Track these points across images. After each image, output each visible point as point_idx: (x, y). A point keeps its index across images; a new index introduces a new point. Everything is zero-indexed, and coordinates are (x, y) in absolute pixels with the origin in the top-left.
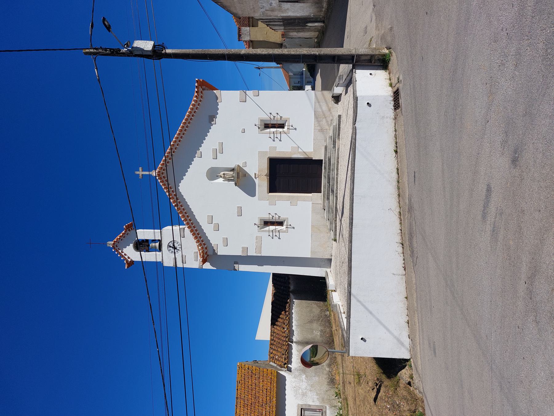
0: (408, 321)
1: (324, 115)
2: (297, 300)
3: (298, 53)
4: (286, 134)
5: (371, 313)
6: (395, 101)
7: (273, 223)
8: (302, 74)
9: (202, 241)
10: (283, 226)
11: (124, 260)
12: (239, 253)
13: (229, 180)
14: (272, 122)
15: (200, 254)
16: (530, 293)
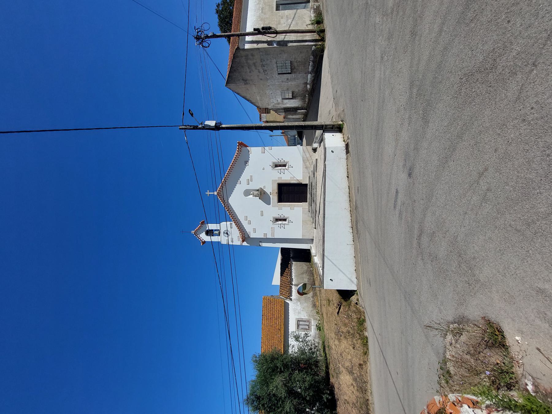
0: (356, 269)
1: (308, 159)
2: (294, 262)
3: (293, 125)
5: (335, 266)
6: (346, 149)
7: (280, 220)
8: (294, 136)
9: (242, 230)
10: (286, 221)
11: (200, 241)
12: (262, 236)
13: (256, 196)
14: (279, 164)
15: (241, 237)
16: (419, 244)
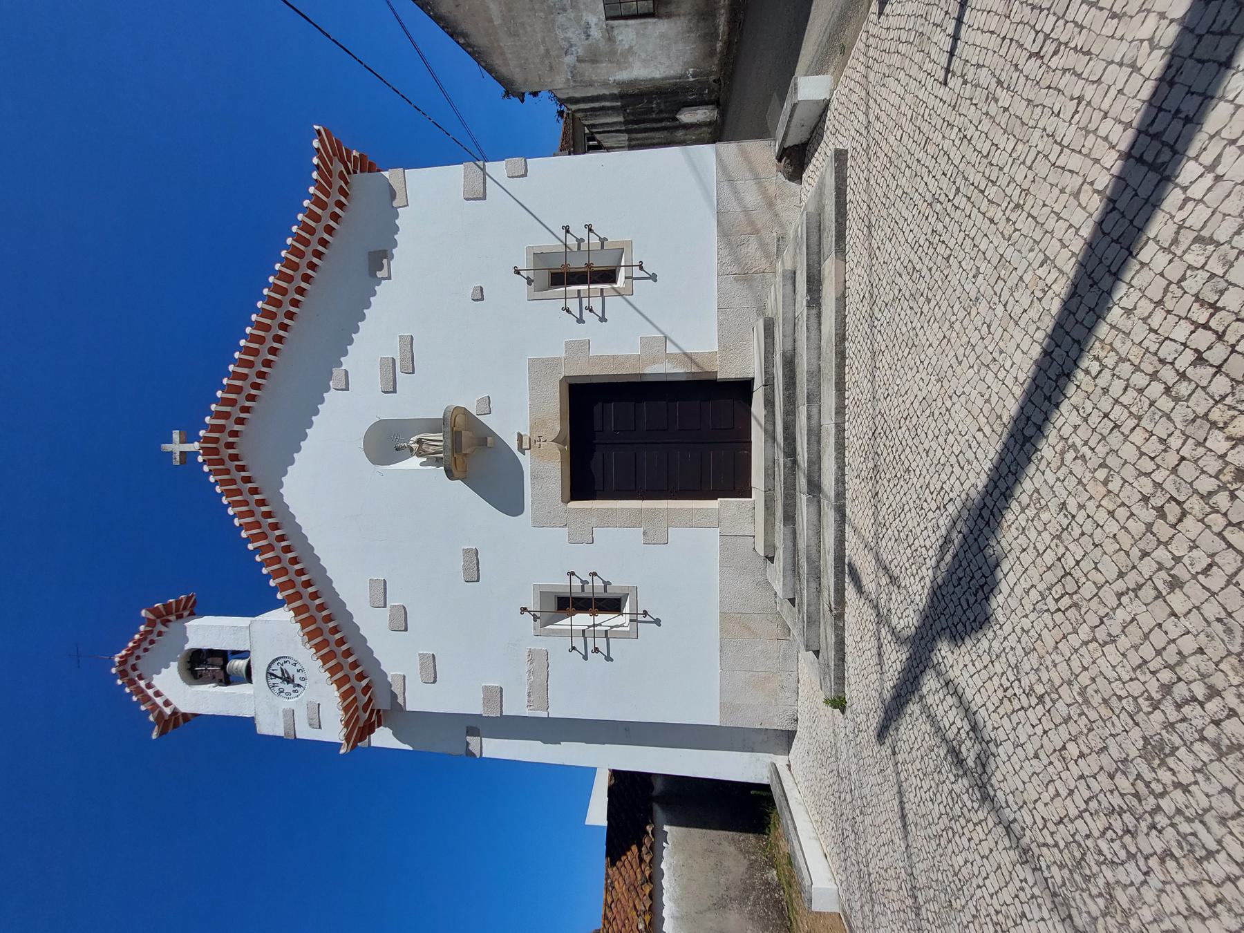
1: (752, 223)
2: (674, 828)
4: (622, 295)
11: (147, 713)
12: (473, 705)
